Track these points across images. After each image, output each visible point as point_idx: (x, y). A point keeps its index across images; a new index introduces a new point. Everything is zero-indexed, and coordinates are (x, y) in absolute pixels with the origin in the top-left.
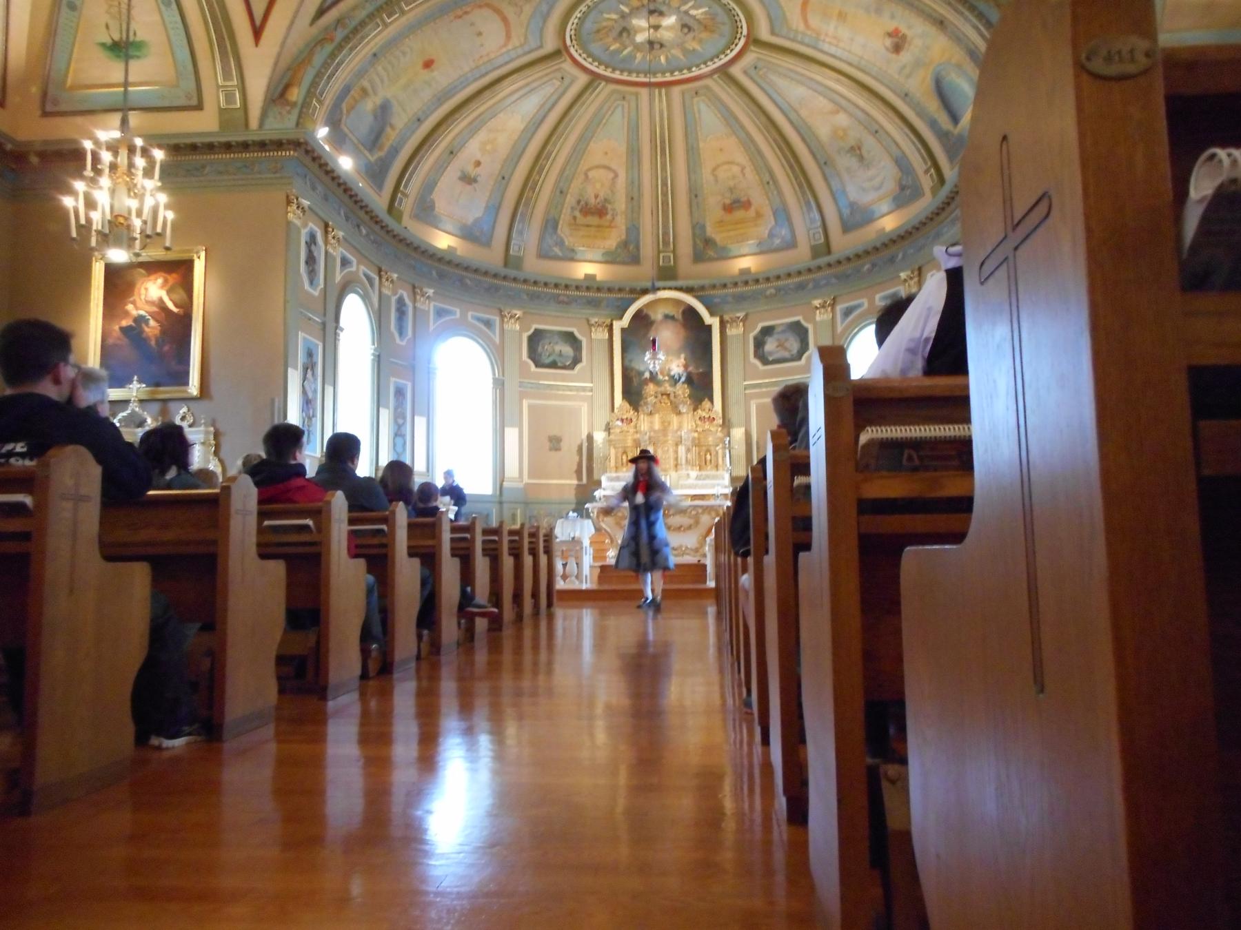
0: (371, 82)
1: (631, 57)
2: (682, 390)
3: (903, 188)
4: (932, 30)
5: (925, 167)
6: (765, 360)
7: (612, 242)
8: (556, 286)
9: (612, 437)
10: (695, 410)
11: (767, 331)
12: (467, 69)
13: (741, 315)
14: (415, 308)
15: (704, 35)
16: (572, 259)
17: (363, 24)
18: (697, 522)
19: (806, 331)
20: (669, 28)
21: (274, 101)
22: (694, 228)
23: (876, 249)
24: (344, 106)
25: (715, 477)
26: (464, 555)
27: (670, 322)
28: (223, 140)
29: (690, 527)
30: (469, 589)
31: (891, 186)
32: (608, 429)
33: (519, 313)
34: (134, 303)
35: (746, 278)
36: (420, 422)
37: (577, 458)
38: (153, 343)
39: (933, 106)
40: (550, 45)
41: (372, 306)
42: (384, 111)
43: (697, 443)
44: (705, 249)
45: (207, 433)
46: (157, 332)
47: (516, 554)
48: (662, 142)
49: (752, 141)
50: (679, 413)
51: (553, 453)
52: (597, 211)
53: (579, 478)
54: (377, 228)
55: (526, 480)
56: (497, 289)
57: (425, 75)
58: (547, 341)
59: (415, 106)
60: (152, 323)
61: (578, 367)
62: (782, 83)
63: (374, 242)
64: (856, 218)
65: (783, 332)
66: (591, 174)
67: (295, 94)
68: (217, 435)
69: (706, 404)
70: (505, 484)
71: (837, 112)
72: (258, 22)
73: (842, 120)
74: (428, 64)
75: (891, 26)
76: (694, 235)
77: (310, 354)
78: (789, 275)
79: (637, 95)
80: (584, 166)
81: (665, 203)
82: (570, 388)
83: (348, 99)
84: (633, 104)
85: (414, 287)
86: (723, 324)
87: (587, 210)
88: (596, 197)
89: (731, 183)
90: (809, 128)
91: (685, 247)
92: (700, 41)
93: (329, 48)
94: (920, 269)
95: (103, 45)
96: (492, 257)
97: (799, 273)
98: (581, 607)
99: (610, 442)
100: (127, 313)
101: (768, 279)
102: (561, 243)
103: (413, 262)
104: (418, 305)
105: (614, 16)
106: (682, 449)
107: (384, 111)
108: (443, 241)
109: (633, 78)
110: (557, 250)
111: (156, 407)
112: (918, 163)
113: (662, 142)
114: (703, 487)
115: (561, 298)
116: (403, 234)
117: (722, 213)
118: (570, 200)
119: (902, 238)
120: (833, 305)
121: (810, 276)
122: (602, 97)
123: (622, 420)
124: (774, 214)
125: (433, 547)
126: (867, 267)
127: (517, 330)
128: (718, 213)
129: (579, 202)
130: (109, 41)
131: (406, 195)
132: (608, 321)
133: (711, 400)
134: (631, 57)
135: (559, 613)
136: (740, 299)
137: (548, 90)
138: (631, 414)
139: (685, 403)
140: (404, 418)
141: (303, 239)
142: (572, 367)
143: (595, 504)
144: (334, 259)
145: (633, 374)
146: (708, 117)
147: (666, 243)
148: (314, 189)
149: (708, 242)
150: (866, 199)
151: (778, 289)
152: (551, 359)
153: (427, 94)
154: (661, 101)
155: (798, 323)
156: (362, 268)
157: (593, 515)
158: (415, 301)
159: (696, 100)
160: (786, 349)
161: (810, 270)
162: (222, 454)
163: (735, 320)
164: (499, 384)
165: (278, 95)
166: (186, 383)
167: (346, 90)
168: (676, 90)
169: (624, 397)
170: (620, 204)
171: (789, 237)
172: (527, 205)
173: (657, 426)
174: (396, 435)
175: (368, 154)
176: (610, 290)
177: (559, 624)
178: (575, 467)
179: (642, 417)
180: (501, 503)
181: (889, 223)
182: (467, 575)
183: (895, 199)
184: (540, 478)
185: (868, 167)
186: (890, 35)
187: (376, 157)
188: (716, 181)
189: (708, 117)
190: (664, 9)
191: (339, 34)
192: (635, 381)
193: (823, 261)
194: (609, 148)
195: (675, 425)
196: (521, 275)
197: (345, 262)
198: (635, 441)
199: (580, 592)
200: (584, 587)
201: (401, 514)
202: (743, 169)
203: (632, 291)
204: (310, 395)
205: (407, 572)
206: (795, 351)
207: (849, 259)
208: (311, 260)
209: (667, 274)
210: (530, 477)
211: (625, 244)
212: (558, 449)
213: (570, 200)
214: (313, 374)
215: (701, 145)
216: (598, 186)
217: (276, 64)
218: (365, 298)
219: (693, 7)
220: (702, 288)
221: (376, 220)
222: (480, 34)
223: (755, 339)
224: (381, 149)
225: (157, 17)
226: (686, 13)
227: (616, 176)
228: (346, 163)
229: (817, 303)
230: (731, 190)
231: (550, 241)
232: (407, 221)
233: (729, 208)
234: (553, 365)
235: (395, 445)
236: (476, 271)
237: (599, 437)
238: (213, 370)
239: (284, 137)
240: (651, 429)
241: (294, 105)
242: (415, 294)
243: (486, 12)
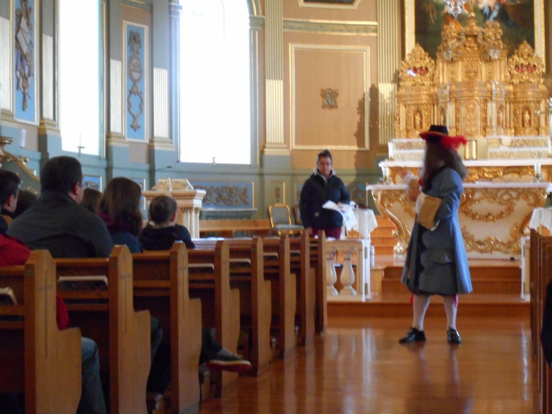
2: (494, 31)
9: (402, 91)
10: (510, 55)
18: (510, 210)
25: (535, 144)
26: (205, 292)
29: (500, 216)
30: (213, 331)
32: (397, 80)
36: (160, 76)
37: (358, 118)
43: (512, 99)
47: (274, 276)
50: (489, 61)
51: (327, 111)
53: (361, 143)
55: (293, 146)
69: (525, 48)
70: (267, 151)
82: (348, 28)
98: (360, 327)
99: (399, 98)
106: (492, 107)
123: (415, 70)
125: (166, 289)
133: (532, 42)
135: (330, 333)
138: (427, 61)
139: (495, 47)
140: (141, 72)
143: (379, 186)
145: (429, 8)
157: (377, 201)
169: (418, 40)
173: (460, 77)
174: (131, 92)
177: (331, 350)
178: (355, 129)
179: (441, 65)
180: (261, 175)
182: (211, 317)
192: (432, 18)
198: (430, 96)
199: (360, 305)
200: (363, 299)
201: (125, 258)
204: (25, 49)
205: (134, 331)
210: (297, 143)
212: (334, 106)
214: (29, 24)
235: (129, 104)
237: (386, 89)
240: (453, 81)
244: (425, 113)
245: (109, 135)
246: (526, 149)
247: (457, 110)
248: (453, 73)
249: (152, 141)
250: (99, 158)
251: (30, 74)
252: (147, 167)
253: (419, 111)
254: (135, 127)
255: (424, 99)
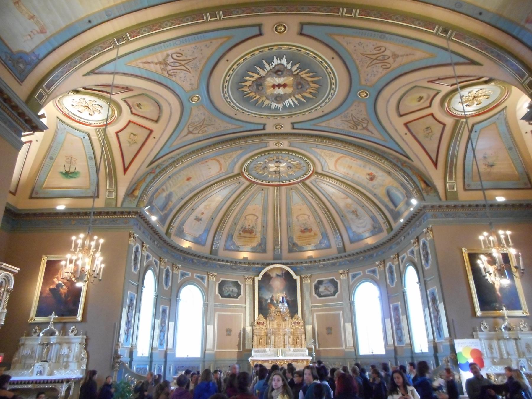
0: (166, 187)
1: (267, 176)
3: (374, 228)
4: (386, 175)
5: (383, 221)
6: (320, 296)
7: (255, 244)
8: (231, 262)
11: (320, 283)
12: (203, 180)
13: (309, 275)
14: (173, 273)
15: (296, 170)
16: (238, 251)
17: (167, 167)
19: (337, 283)
20: (283, 167)
21: (128, 195)
22: (288, 238)
23: (365, 251)
24: (155, 196)
25: (302, 351)
27: (279, 277)
28: (106, 211)
31: (369, 226)
33: (215, 274)
34: (57, 278)
35: (310, 260)
36: (172, 324)
37: (238, 339)
38: (63, 296)
39: (386, 200)
40: (236, 171)
41: (156, 274)
42: (169, 196)
43: (293, 334)
44: (293, 247)
45: (82, 338)
46: (66, 291)
48: (277, 206)
49: (313, 207)
52: (249, 232)
53: (239, 348)
54: (161, 241)
55: (216, 350)
56: (207, 263)
57: (187, 182)
58: (227, 285)
59: (181, 194)
60: (64, 287)
61: (240, 297)
62: (323, 185)
63: (160, 247)
64: (356, 239)
65: (327, 283)
66: (247, 217)
67: (137, 193)
68: (86, 340)
69: (296, 316)
70: (207, 352)
71: (347, 198)
72: (126, 166)
73: (349, 201)
74: (188, 179)
75: (369, 172)
76: (289, 242)
77: (131, 300)
78: (329, 260)
79: (268, 189)
80: (245, 214)
81: (277, 229)
83: (157, 193)
84: (266, 192)
85: (173, 264)
86: (301, 278)
87: (245, 231)
88: (249, 226)
89: (304, 222)
90: (336, 203)
91: (285, 247)
92: (294, 172)
93: (153, 175)
94: (384, 261)
95: (61, 173)
96: (205, 251)
97: (333, 259)
100: (54, 282)
101: (320, 261)
102: (234, 244)
103: (173, 254)
104: (174, 272)
105: (262, 163)
106: (286, 337)
107: (169, 196)
108: (186, 244)
109: (267, 183)
110: (232, 247)
111: (61, 325)
112: (380, 219)
113: (277, 206)
114: (296, 356)
115: (233, 267)
116: (171, 243)
117: (300, 233)
118: (239, 227)
119: (375, 247)
120: (348, 273)
121: (336, 261)
122: (254, 189)
124: (322, 234)
126: (361, 258)
127: (214, 281)
128: (299, 233)
129: (242, 228)
130: (64, 171)
131: (173, 227)
132: (252, 277)
134: (267, 176)
136: (308, 268)
137: (233, 187)
140: (165, 323)
141: (134, 250)
142: (237, 297)
144: (144, 256)
145: (263, 300)
146: (296, 198)
147: (277, 245)
148: (140, 229)
149: (295, 244)
150: (360, 231)
151: (324, 265)
152: (228, 294)
153: (186, 189)
154: (277, 191)
155: (333, 280)
156: (154, 258)
158: (173, 270)
159: (291, 191)
160: (329, 291)
161: (337, 258)
162: (88, 349)
163: (306, 277)
164: (206, 305)
165: (130, 193)
166: (76, 315)
167: (157, 190)
168: (283, 188)
170: (259, 228)
171: (328, 244)
172: (221, 229)
173: (275, 326)
174: (161, 331)
175: (161, 212)
176: (254, 264)
178: (237, 343)
181: (370, 241)
183: (372, 232)
184: (222, 349)
185: (360, 219)
186: (369, 175)
187: (164, 213)
188: (298, 221)
189: (296, 198)
190: (281, 161)
191: (158, 170)
192: (264, 304)
193: (343, 254)
194: (255, 206)
195: (283, 326)
196: (217, 258)
197: (148, 257)
198: (265, 332)
202: (309, 216)
203: (263, 264)
204: (130, 319)
206: (332, 292)
207: (353, 254)
208: (136, 259)
209: (277, 258)
210: (217, 348)
211: (260, 245)
213: (239, 227)
215: (292, 207)
216: (250, 222)
217: (131, 182)
218: (154, 272)
219: (292, 161)
220: (292, 264)
221: (161, 238)
222: (210, 168)
223: (315, 286)
224: (166, 210)
225: (86, 164)
226: (290, 162)
227: (258, 218)
228: (154, 218)
229: (340, 271)
230: (304, 224)
231: (229, 243)
232: (173, 237)
233: (303, 231)
234: (229, 296)
236: (199, 256)
237: (248, 329)
238: (89, 309)
239: (131, 210)
241: (137, 197)
242: (173, 267)
243: (214, 161)
244: (263, 339)
245: (152, 348)
246: (298, 353)
247: (275, 338)
248: (273, 324)
249: (167, 349)
250: (148, 357)
251: (130, 328)
252: (164, 360)
253: (261, 338)
254: (161, 344)
255: (263, 334)
